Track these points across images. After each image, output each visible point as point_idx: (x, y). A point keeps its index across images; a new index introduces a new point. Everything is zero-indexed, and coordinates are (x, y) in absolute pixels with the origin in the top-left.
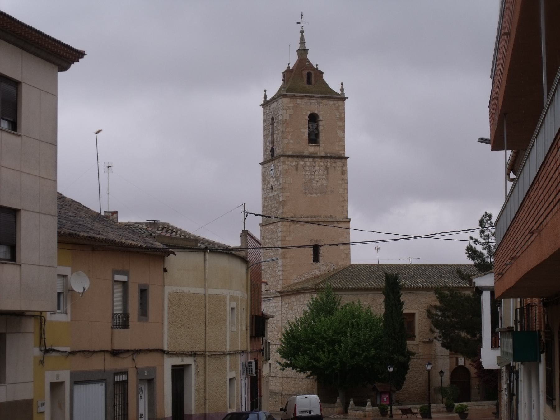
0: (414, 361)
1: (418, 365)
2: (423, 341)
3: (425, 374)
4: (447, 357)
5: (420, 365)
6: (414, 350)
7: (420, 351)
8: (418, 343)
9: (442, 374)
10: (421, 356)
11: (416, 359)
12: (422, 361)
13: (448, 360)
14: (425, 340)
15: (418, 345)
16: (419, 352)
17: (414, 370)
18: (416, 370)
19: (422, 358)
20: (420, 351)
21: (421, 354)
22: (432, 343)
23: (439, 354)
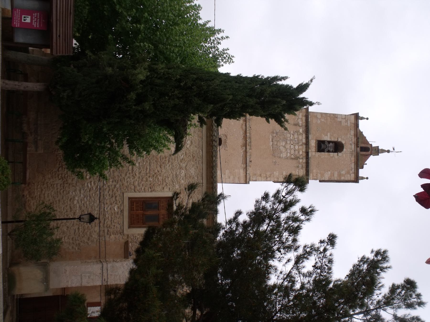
0: (95, 226)
1: (88, 233)
2: (129, 242)
3: (73, 247)
4: (105, 280)
5: (89, 238)
6: (114, 226)
7: (112, 236)
8: (125, 232)
9: (86, 218)
10: (103, 239)
11: (98, 231)
12: (95, 240)
13: (99, 283)
14: (130, 245)
15: (122, 233)
16: (111, 235)
17: (80, 227)
18: (81, 230)
19: (101, 241)
20: (112, 236)
21: (107, 239)
22: (125, 258)
23: (109, 265)
